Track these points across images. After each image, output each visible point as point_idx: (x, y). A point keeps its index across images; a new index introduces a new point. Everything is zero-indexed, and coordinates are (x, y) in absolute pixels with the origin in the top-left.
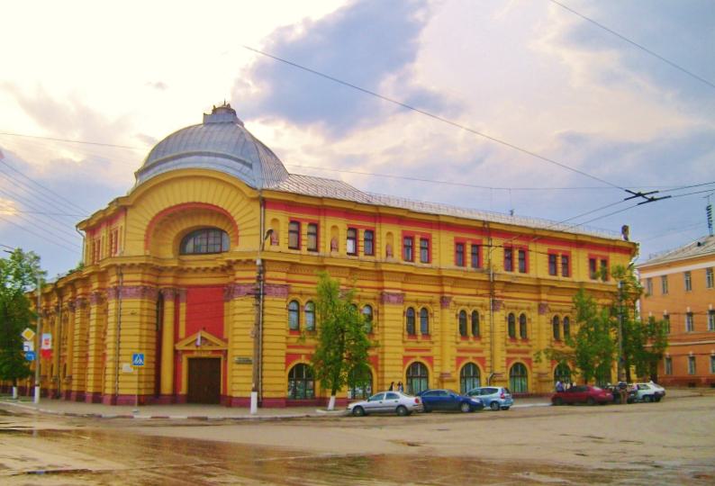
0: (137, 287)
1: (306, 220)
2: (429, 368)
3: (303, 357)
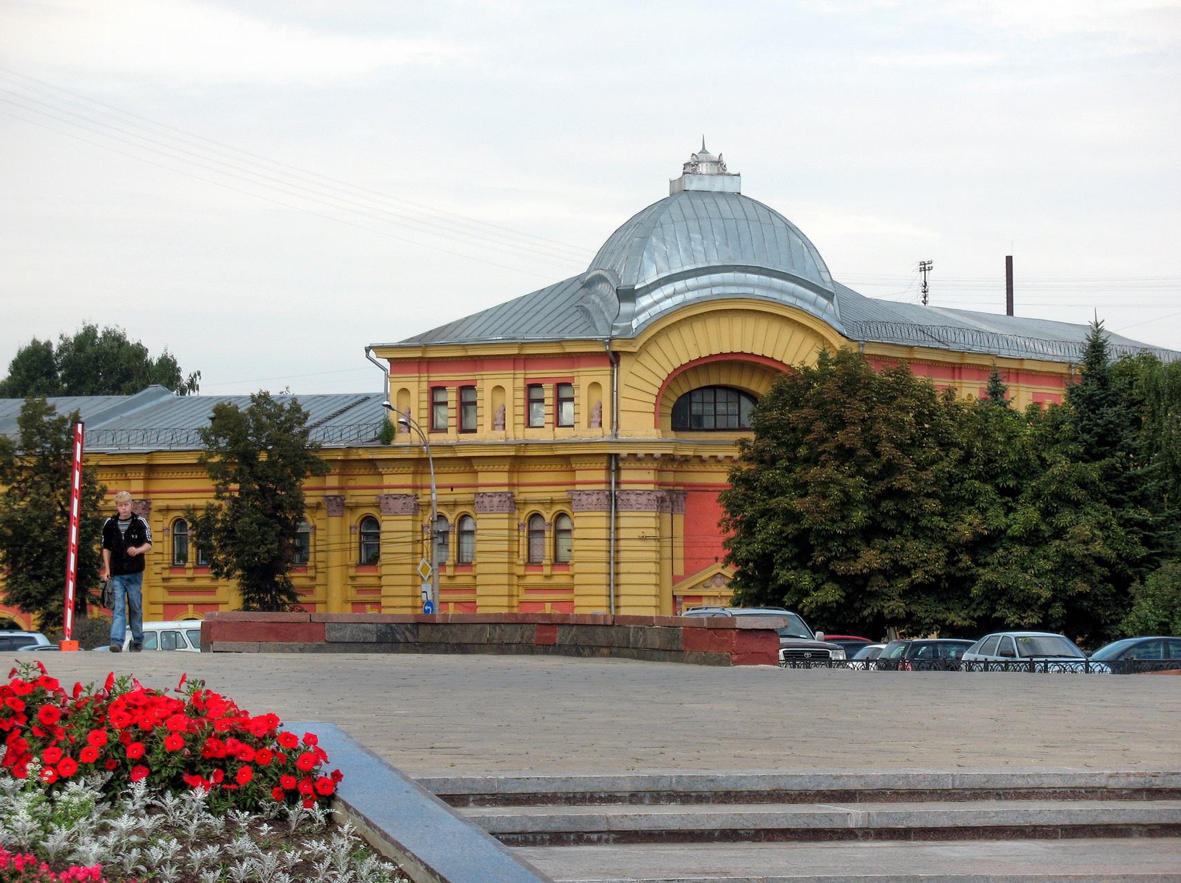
0: (599, 492)
3: (548, 606)
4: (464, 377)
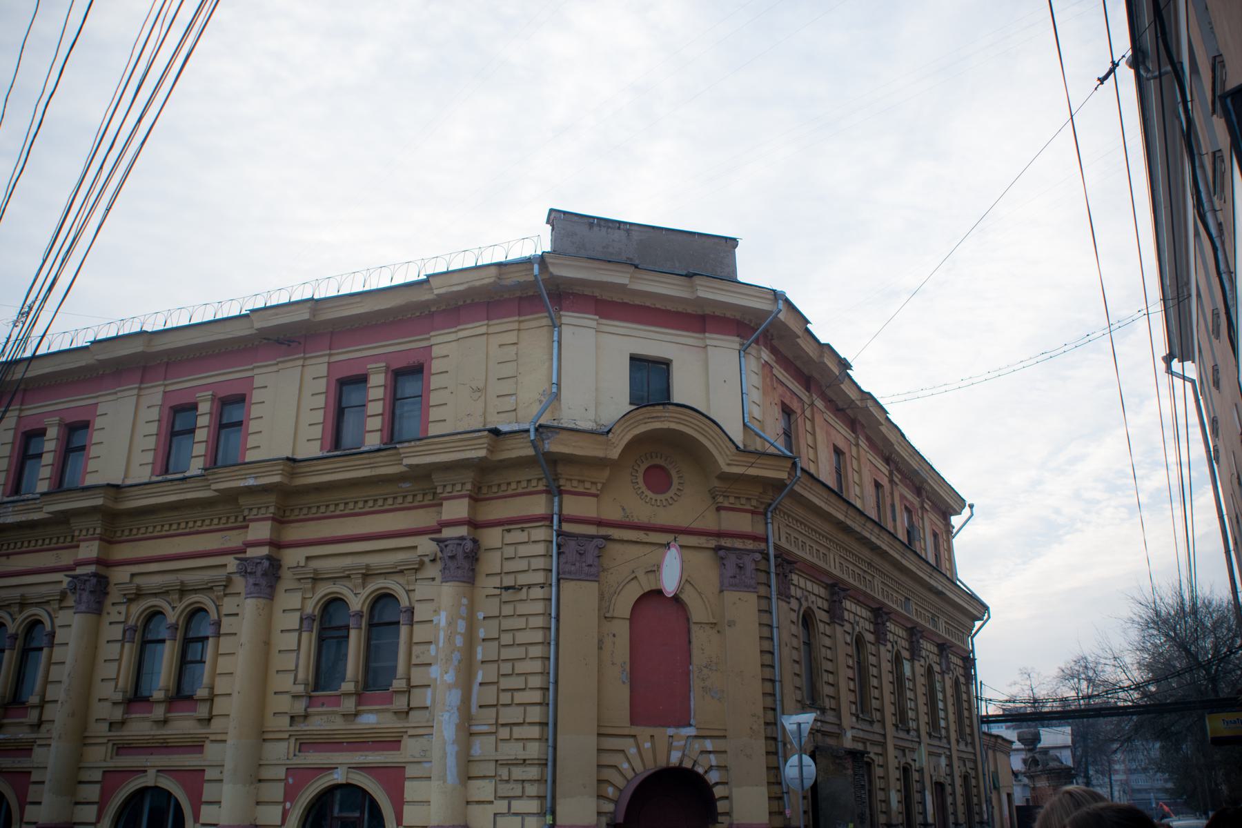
4: (400, 347)
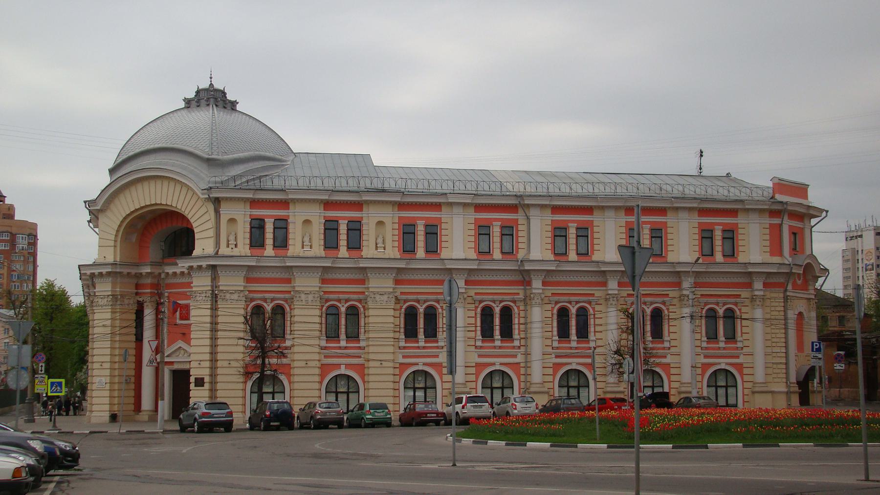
1: (270, 217)
2: (590, 377)
